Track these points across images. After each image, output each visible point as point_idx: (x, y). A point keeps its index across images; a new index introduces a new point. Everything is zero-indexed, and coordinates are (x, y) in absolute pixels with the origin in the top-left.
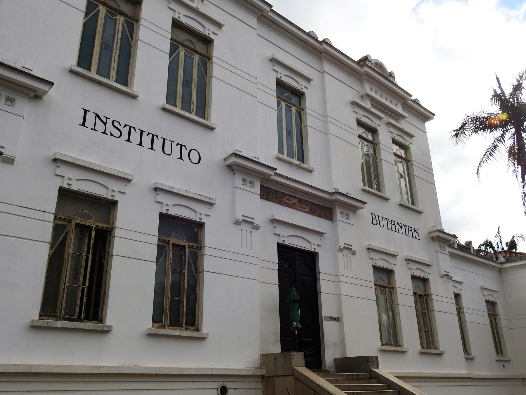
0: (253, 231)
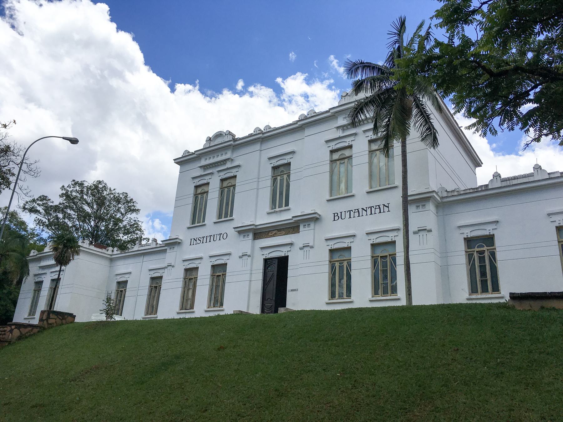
0: (427, 233)
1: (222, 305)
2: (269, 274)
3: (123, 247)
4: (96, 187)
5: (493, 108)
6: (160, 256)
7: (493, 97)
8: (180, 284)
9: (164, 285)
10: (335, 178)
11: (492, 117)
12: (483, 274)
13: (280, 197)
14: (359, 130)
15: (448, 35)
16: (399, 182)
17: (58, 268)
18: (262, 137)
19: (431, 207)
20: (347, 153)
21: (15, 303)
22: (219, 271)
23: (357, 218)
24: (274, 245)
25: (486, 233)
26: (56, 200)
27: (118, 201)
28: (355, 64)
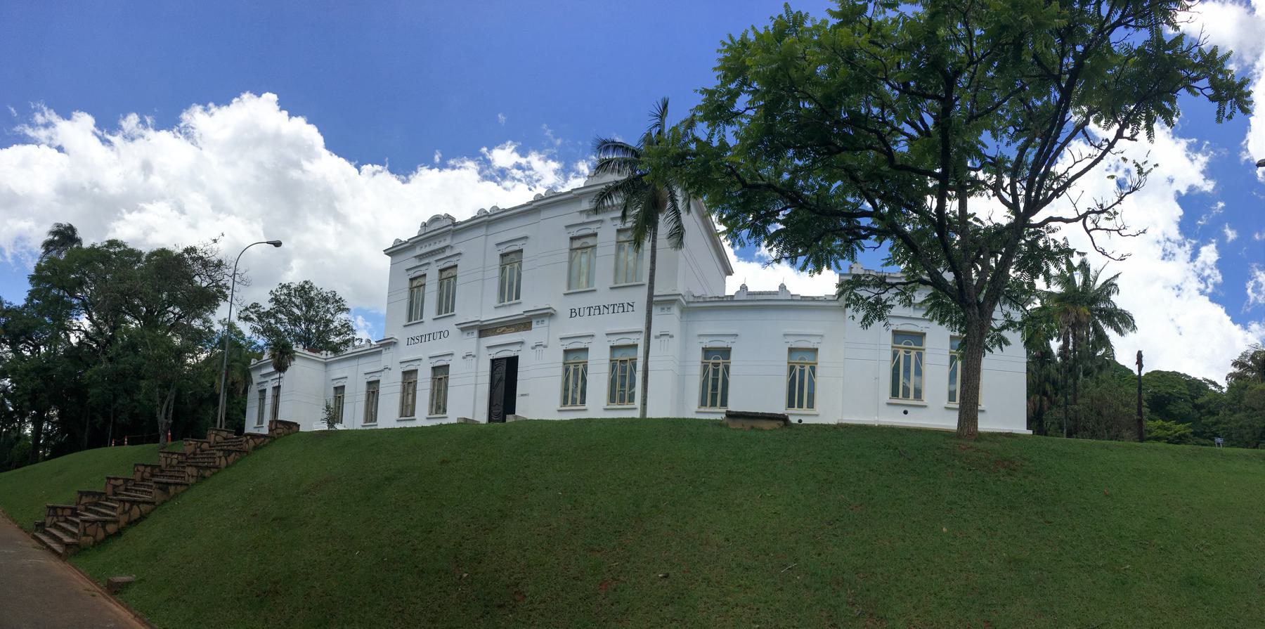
1: (445, 411)
2: (497, 377)
3: (335, 349)
4: (303, 288)
5: (744, 219)
6: (375, 358)
7: (745, 208)
8: (399, 388)
9: (382, 390)
10: (575, 274)
11: (740, 229)
12: (715, 387)
13: (510, 289)
14: (606, 217)
15: (708, 131)
16: (646, 280)
17: (277, 376)
18: (488, 220)
19: (675, 310)
20: (590, 241)
21: (244, 413)
22: (440, 373)
23: (597, 316)
24: (502, 345)
25: (725, 345)
26: (267, 306)
27: (326, 300)
28: (605, 142)
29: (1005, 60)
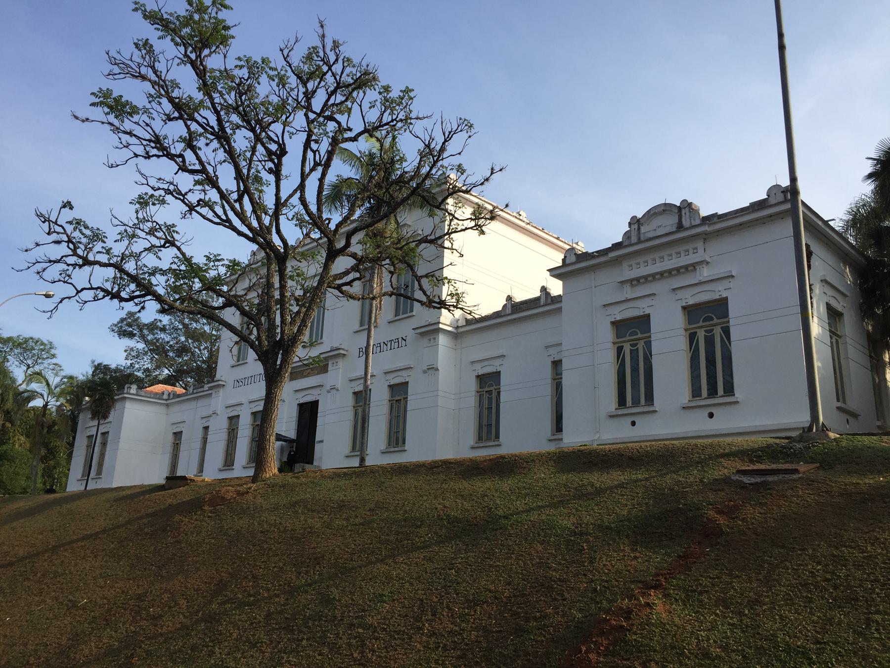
10: (486, 363)
12: (490, 409)
25: (716, 296)
29: (174, 231)
